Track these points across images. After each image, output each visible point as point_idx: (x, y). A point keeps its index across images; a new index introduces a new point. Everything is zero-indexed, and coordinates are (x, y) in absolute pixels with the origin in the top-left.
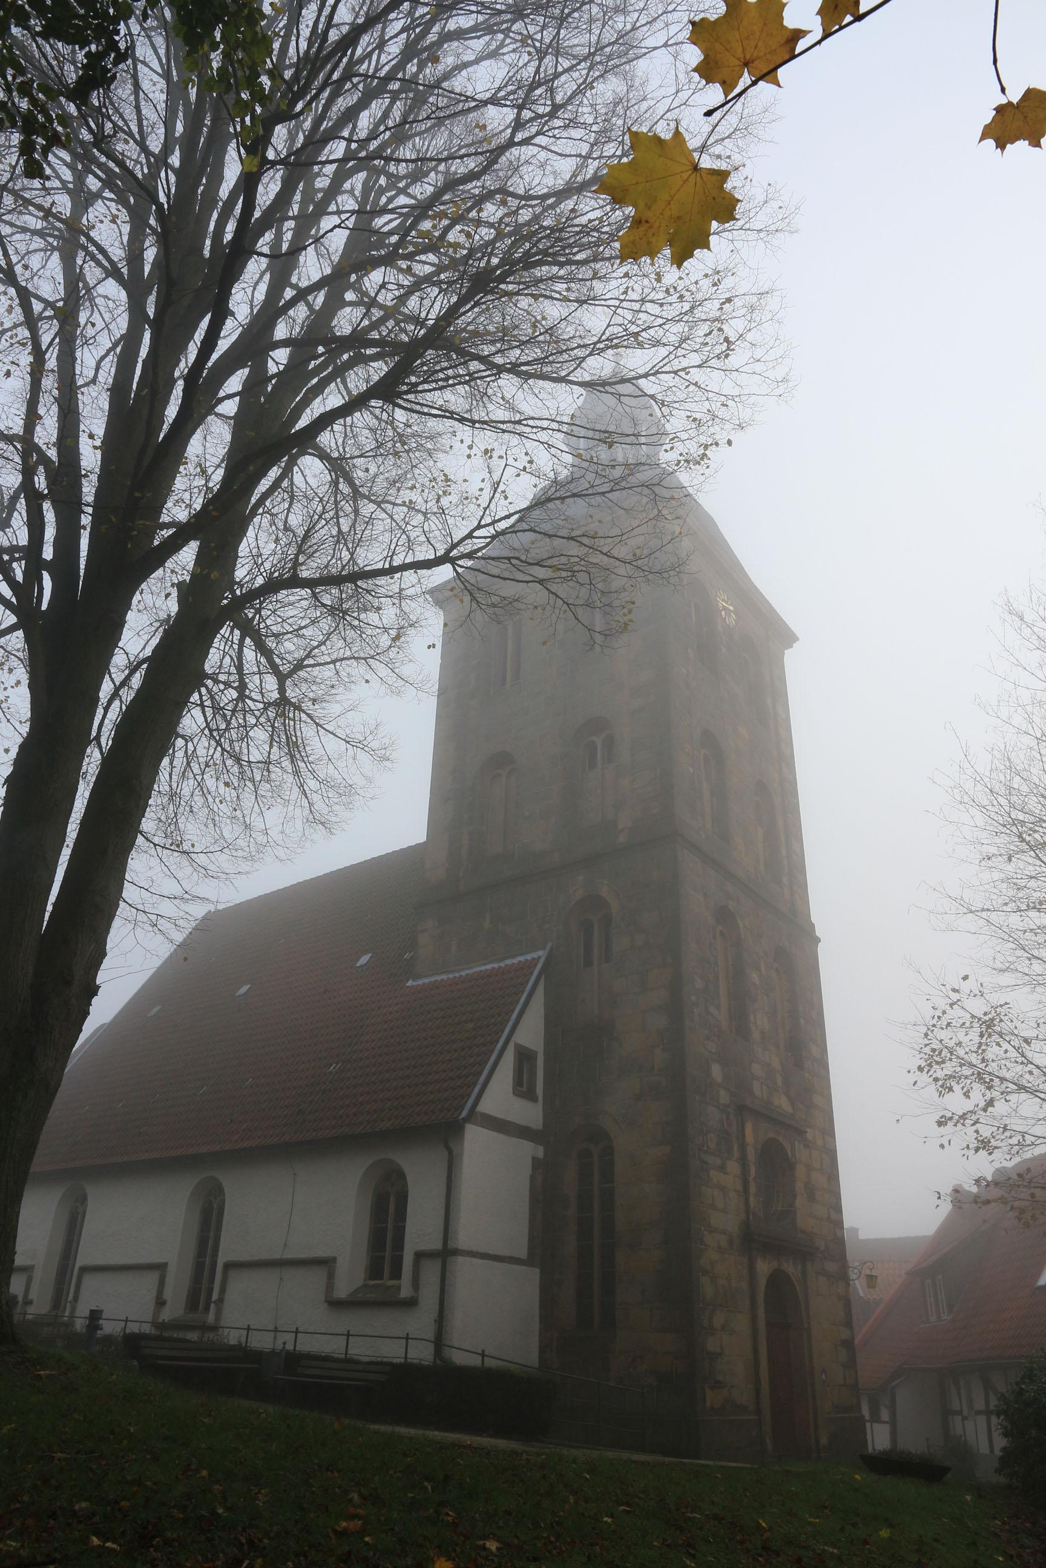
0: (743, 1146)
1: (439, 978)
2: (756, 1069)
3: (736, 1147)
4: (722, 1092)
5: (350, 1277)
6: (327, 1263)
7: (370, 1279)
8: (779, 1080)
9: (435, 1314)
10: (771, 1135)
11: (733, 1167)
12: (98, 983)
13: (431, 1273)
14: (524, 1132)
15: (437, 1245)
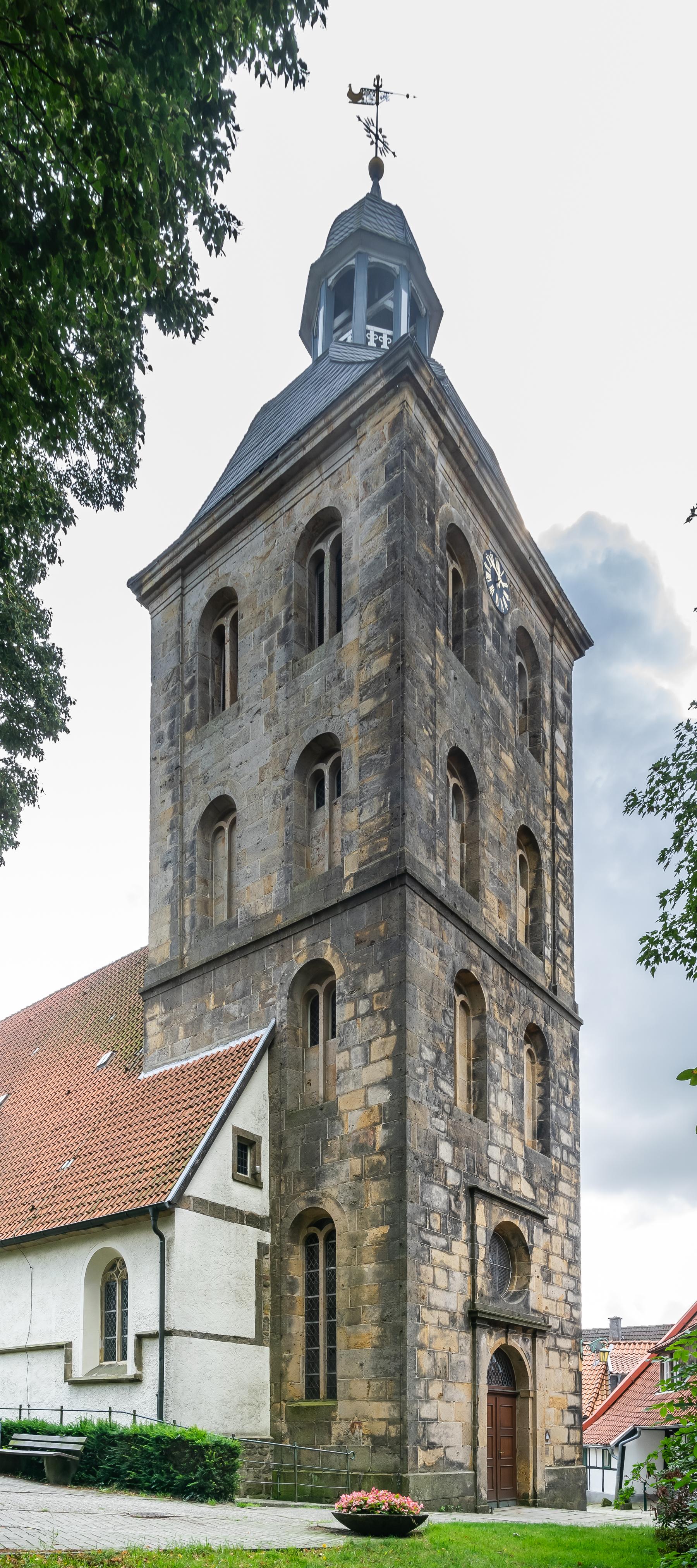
0: (472, 1229)
1: (167, 1068)
2: (494, 1152)
5: (86, 1359)
6: (65, 1348)
7: (106, 1360)
8: (521, 1165)
9: (157, 1390)
11: (460, 1248)
13: (151, 1351)
14: (252, 1220)
15: (155, 1328)
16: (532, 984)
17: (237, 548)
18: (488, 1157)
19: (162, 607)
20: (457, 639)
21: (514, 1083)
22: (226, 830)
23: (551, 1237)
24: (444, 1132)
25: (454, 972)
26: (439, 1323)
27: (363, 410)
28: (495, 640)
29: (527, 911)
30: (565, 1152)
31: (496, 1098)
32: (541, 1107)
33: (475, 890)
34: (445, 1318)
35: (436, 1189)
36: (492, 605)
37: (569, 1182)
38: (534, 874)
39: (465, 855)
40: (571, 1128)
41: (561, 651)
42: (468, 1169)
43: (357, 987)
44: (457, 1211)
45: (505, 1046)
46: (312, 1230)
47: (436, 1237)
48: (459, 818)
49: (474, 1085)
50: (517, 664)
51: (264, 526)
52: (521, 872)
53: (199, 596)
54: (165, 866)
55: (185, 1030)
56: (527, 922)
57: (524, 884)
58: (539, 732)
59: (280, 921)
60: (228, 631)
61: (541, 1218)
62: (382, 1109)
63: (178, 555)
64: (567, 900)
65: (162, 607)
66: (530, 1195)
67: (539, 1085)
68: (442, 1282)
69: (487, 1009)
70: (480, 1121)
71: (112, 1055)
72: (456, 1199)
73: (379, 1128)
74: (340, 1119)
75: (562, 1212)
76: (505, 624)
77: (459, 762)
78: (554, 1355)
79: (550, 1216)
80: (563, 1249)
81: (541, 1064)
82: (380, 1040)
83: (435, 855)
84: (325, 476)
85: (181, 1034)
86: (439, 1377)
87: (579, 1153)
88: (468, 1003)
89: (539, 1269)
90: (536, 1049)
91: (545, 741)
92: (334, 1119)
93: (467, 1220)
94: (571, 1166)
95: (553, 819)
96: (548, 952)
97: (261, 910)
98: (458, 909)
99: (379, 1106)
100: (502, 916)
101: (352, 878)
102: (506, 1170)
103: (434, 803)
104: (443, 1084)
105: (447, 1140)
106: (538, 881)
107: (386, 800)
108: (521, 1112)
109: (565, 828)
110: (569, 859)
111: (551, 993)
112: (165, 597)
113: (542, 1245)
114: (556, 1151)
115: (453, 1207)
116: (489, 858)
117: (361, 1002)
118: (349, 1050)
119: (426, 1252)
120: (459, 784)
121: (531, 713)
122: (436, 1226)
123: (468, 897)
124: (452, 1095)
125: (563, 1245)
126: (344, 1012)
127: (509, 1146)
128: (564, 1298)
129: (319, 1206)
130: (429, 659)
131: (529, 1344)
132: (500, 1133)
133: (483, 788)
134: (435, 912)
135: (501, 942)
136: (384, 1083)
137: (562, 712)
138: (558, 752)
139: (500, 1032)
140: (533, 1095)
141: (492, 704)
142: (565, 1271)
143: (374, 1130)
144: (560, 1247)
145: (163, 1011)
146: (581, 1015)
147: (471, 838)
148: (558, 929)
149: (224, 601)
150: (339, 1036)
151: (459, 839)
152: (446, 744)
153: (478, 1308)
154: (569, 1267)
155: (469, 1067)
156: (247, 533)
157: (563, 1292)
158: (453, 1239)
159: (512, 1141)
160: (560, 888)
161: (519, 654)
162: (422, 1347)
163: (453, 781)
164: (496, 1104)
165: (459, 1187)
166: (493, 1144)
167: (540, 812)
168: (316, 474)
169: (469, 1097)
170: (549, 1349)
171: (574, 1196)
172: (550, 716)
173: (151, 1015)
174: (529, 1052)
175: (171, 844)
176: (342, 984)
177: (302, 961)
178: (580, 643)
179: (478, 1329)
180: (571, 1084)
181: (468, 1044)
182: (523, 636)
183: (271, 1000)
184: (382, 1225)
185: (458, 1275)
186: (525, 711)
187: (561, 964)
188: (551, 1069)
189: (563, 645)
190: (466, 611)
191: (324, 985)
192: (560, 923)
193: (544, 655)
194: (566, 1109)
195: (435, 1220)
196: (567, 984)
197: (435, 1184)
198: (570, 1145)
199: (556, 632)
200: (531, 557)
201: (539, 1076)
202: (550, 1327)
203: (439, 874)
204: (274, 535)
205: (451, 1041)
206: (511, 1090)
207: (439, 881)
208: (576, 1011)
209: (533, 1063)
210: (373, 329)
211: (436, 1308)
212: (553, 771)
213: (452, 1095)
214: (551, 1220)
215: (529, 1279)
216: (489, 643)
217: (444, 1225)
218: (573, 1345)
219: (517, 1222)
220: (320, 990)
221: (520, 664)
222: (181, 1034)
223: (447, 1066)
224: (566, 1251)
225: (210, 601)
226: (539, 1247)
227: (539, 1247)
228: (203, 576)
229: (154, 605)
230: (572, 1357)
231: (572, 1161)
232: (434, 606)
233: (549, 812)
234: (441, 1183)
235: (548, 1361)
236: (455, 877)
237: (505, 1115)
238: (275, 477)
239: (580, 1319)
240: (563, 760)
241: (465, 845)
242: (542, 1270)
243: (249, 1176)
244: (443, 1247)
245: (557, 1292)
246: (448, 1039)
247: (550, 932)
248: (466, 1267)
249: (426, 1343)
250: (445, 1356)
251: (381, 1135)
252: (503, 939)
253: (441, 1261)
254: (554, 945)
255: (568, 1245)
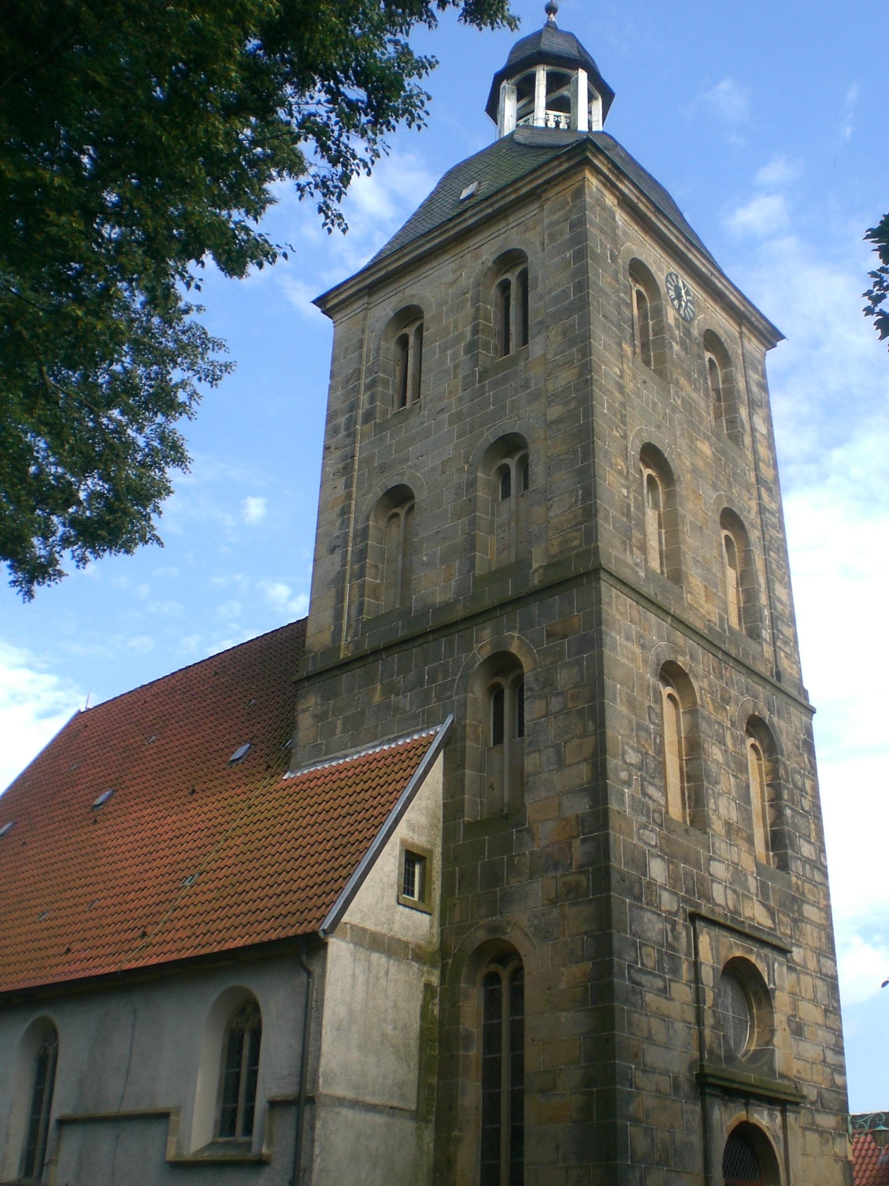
0: (696, 966)
2: (718, 869)
3: (685, 966)
4: (666, 897)
8: (752, 884)
10: (738, 953)
11: (682, 991)
12: (879, 330)
16: (751, 672)
17: (424, 275)
18: (711, 875)
19: (346, 318)
20: (645, 346)
21: (737, 785)
22: (402, 516)
23: (798, 978)
24: (656, 846)
25: (658, 665)
26: (658, 1091)
27: (547, 182)
28: (683, 344)
29: (738, 591)
30: (808, 867)
31: (716, 803)
32: (773, 811)
33: (677, 577)
34: (665, 1084)
35: (648, 916)
36: (677, 316)
37: (815, 904)
38: (743, 554)
39: (664, 541)
40: (813, 835)
41: (753, 345)
42: (687, 892)
43: (549, 683)
44: (675, 944)
45: (722, 742)
46: (493, 967)
47: (650, 977)
48: (656, 506)
49: (689, 789)
50: (707, 360)
51: (453, 259)
52: (728, 551)
53: (385, 308)
54: (332, 550)
55: (344, 724)
56: (738, 603)
57: (732, 565)
58: (736, 418)
59: (460, 612)
60: (411, 340)
61: (784, 952)
62: (581, 820)
63: (366, 278)
64: (783, 578)
65: (346, 318)
66: (768, 922)
67: (768, 785)
68: (660, 1036)
69: (699, 702)
70: (698, 832)
71: (249, 748)
72: (673, 929)
73: (577, 843)
74: (529, 831)
75: (810, 942)
76: (692, 330)
77: (651, 455)
78: (813, 1137)
79: (794, 949)
80: (815, 992)
81: (769, 760)
82: (576, 741)
83: (631, 547)
84: (511, 226)
85: (339, 730)
86: (659, 1163)
87: (826, 867)
88: (676, 695)
89: (784, 1019)
90: (761, 743)
91: (743, 425)
92: (521, 831)
93: (688, 954)
94: (816, 885)
95: (760, 497)
96: (766, 634)
97: (439, 599)
98: (659, 598)
99: (577, 816)
100: (713, 596)
101: (541, 570)
102: (735, 891)
103: (628, 497)
104: (651, 790)
105: (659, 856)
106: (747, 559)
107: (577, 496)
108: (750, 819)
109: (774, 506)
110: (780, 536)
111: (774, 680)
112: (350, 310)
113: (787, 985)
114: (796, 866)
115: (670, 939)
116: (690, 542)
117: (553, 699)
118: (540, 751)
119: (639, 997)
120: (654, 474)
121: (725, 401)
122: (650, 963)
123: (669, 584)
124: (662, 802)
125: (814, 986)
126: (533, 710)
127: (736, 861)
128: (821, 1058)
129: (503, 937)
130: (617, 370)
131: (779, 1119)
132: (723, 846)
133: (679, 477)
134: (634, 603)
135: (710, 629)
136: (583, 790)
137: (759, 397)
138: (758, 435)
139: (716, 726)
140: (763, 798)
141: (683, 399)
142: (821, 1022)
143: (570, 845)
144: (810, 989)
145: (319, 702)
146: (813, 702)
147: (670, 523)
148: (775, 610)
149: (410, 315)
150: (528, 735)
151: (656, 526)
152: (637, 441)
153: (707, 1070)
154: (826, 1016)
155: (681, 769)
156: (435, 264)
157: (819, 1050)
158: (670, 980)
159: (739, 855)
160: (774, 567)
161: (708, 350)
162: (636, 1121)
163: (647, 472)
164: (716, 810)
165: (676, 914)
166: (715, 860)
167: (744, 492)
168: (504, 223)
169: (684, 804)
170: (805, 1129)
171: (824, 922)
172: (746, 402)
173: (304, 707)
174: (753, 746)
175: (340, 529)
176: (531, 679)
177: (486, 653)
178: (770, 336)
179: (708, 1099)
180: (808, 784)
181: (679, 742)
182: (711, 340)
183: (448, 694)
184: (583, 960)
185: (680, 1026)
186: (718, 399)
187: (783, 647)
188: (781, 767)
189: (754, 340)
190: (651, 323)
191: (511, 677)
192: (777, 603)
193: (735, 350)
194: (805, 814)
195: (648, 955)
196: (792, 668)
197: (647, 910)
198: (814, 857)
199: (744, 329)
200: (712, 274)
201: (767, 775)
202: (804, 1097)
203: (637, 565)
204: (461, 267)
205: (658, 740)
206: (733, 793)
207: (637, 573)
208: (806, 698)
209: (759, 759)
210: (552, 113)
211: (653, 1070)
212: (755, 452)
213: (662, 802)
214: (797, 954)
215: (772, 1032)
216: (676, 347)
217: (660, 962)
218: (838, 1123)
219: (753, 959)
220: (506, 683)
221: (710, 360)
222: (339, 730)
223: (655, 769)
224: (819, 995)
225: (395, 315)
226: (782, 989)
227: (782, 989)
228: (389, 295)
229: (338, 316)
230: (838, 1140)
231: (818, 877)
232: (620, 325)
233: (754, 492)
234: (654, 909)
235: (805, 1145)
236: (655, 564)
237: (728, 825)
238: (464, 225)
239: (845, 1088)
240: (765, 442)
241: (663, 531)
242: (789, 1020)
243: (416, 898)
244: (659, 990)
245: (811, 1051)
246: (655, 738)
247: (766, 612)
248: (690, 1015)
249: (641, 1116)
250: (666, 1135)
251: (579, 851)
252: (712, 625)
253: (658, 1008)
254: (773, 626)
255: (822, 987)
